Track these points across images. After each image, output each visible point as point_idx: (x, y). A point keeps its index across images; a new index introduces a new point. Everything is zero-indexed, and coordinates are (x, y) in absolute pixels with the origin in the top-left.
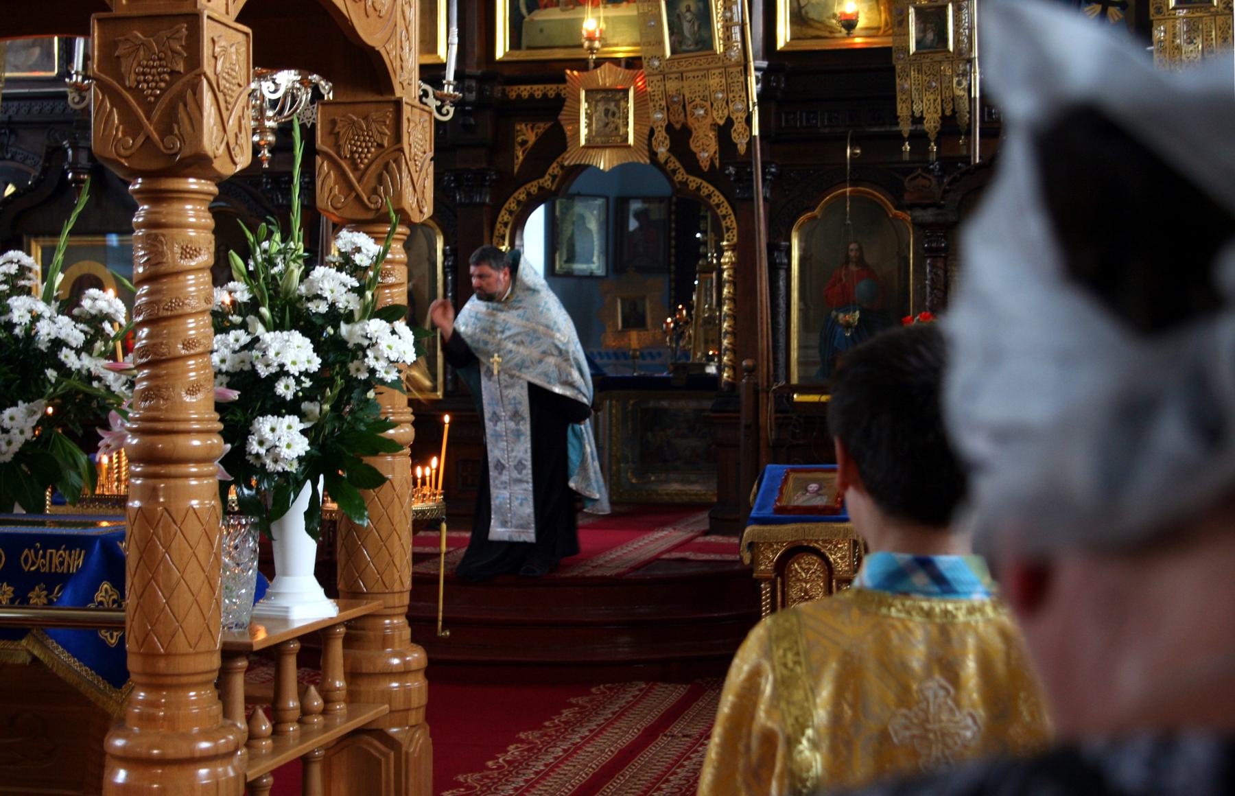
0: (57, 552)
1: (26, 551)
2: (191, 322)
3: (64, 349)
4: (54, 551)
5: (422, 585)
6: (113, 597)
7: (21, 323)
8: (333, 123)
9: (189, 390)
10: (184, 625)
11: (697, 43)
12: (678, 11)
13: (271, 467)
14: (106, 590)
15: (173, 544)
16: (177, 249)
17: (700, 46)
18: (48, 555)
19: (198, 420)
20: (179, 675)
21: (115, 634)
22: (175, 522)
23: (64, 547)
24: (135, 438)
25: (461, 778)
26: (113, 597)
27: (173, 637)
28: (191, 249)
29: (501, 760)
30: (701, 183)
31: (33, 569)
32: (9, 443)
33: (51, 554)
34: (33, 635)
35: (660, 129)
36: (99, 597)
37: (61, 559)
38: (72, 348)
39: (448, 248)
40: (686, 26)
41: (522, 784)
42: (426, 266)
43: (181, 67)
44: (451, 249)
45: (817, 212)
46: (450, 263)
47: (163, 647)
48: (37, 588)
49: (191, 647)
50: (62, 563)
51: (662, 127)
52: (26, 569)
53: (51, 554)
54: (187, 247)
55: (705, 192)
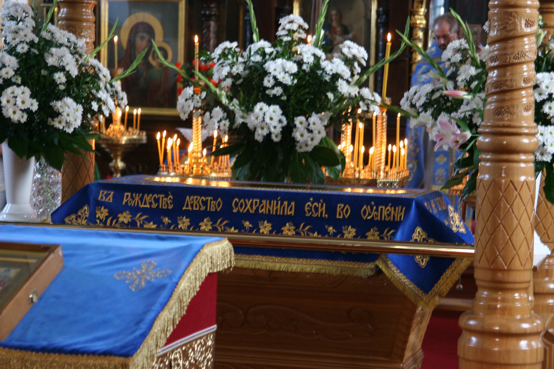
0: (385, 208)
1: (365, 207)
2: (525, 67)
3: (340, 80)
4: (384, 207)
6: (423, 237)
7: (309, 63)
9: (525, 109)
10: (519, 252)
13: (539, 158)
14: (419, 232)
15: (515, 203)
16: (523, 22)
18: (380, 209)
19: (527, 128)
20: (515, 283)
21: (424, 260)
22: (516, 189)
23: (390, 205)
24: (486, 138)
26: (423, 237)
27: (512, 259)
28: (531, 21)
31: (369, 218)
32: (312, 139)
33: (382, 209)
34: (382, 258)
36: (415, 236)
37: (388, 212)
38: (344, 80)
39: (381, 9)
42: (362, 23)
44: (384, 10)
46: (382, 21)
47: (506, 265)
48: (372, 230)
49: (522, 266)
50: (389, 215)
52: (365, 218)
53: (382, 209)
54: (529, 20)
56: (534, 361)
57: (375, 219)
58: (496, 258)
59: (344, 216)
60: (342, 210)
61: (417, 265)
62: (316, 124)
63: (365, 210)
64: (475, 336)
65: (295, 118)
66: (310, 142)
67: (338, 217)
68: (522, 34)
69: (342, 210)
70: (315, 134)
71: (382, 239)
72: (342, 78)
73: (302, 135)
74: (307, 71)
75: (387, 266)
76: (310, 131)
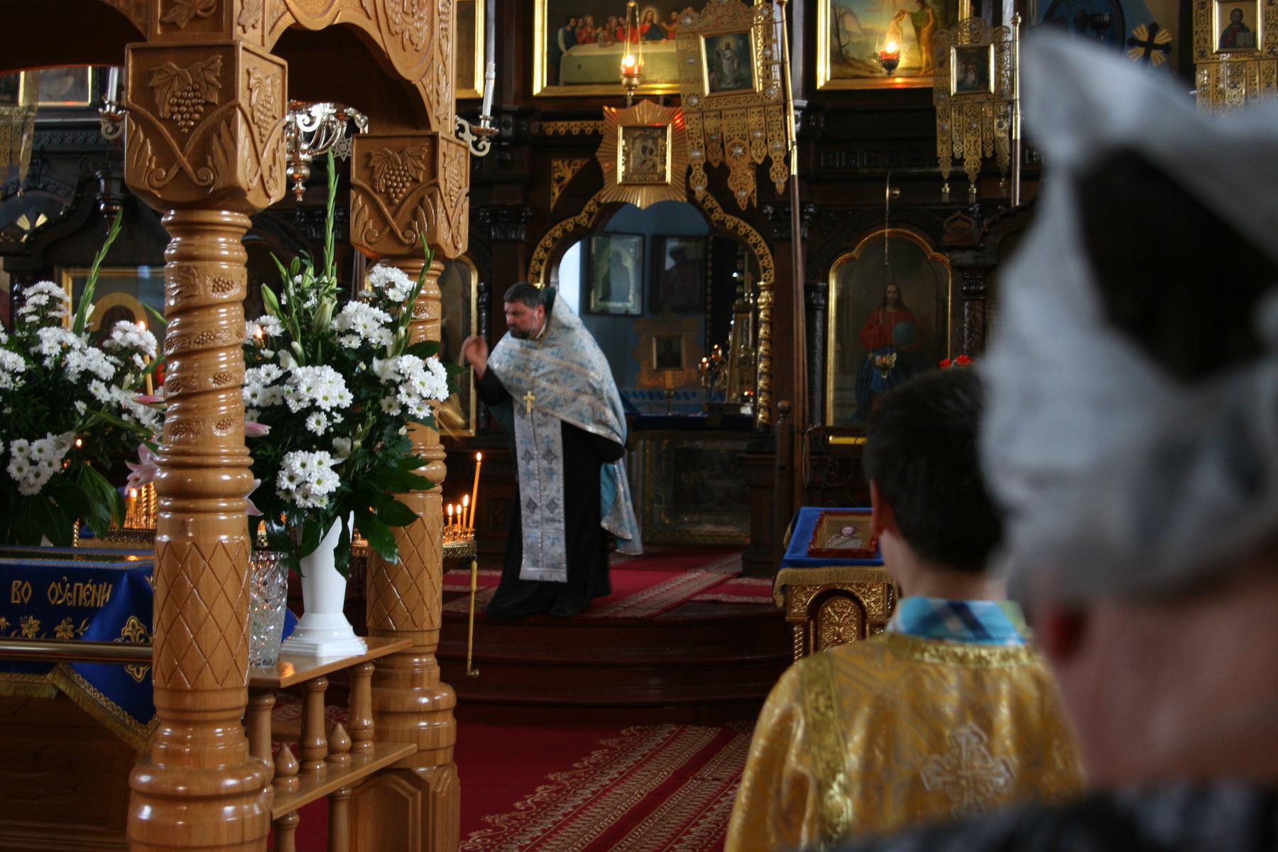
1: (53, 585)
2: (222, 356)
3: (94, 381)
5: (452, 624)
6: (140, 632)
8: (369, 156)
9: (219, 424)
11: (736, 81)
12: (717, 49)
16: (209, 282)
17: (739, 84)
19: (228, 455)
22: (203, 557)
23: (91, 580)
25: (489, 819)
26: (140, 632)
28: (223, 282)
29: (529, 801)
30: (739, 223)
31: (60, 602)
32: (37, 475)
33: (78, 587)
35: (697, 167)
36: (126, 631)
37: (88, 593)
38: (102, 381)
39: (482, 284)
40: (725, 63)
41: (551, 826)
43: (215, 99)
45: (855, 253)
48: (63, 622)
50: (89, 597)
51: (700, 165)
52: (53, 603)
53: (78, 587)
54: (219, 280)
55: (742, 231)
56: (237, 840)
57: (69, 604)
58: (174, 670)
59: (22, 599)
60: (20, 590)
61: (129, 678)
62: (45, 450)
63: (54, 589)
64: (150, 804)
65: (11, 443)
66: (32, 479)
67: (13, 601)
68: (208, 302)
69: (20, 590)
70: (43, 466)
71: (77, 636)
72: (97, 377)
73: (20, 469)
74: (50, 369)
75: (71, 682)
76: (33, 463)
